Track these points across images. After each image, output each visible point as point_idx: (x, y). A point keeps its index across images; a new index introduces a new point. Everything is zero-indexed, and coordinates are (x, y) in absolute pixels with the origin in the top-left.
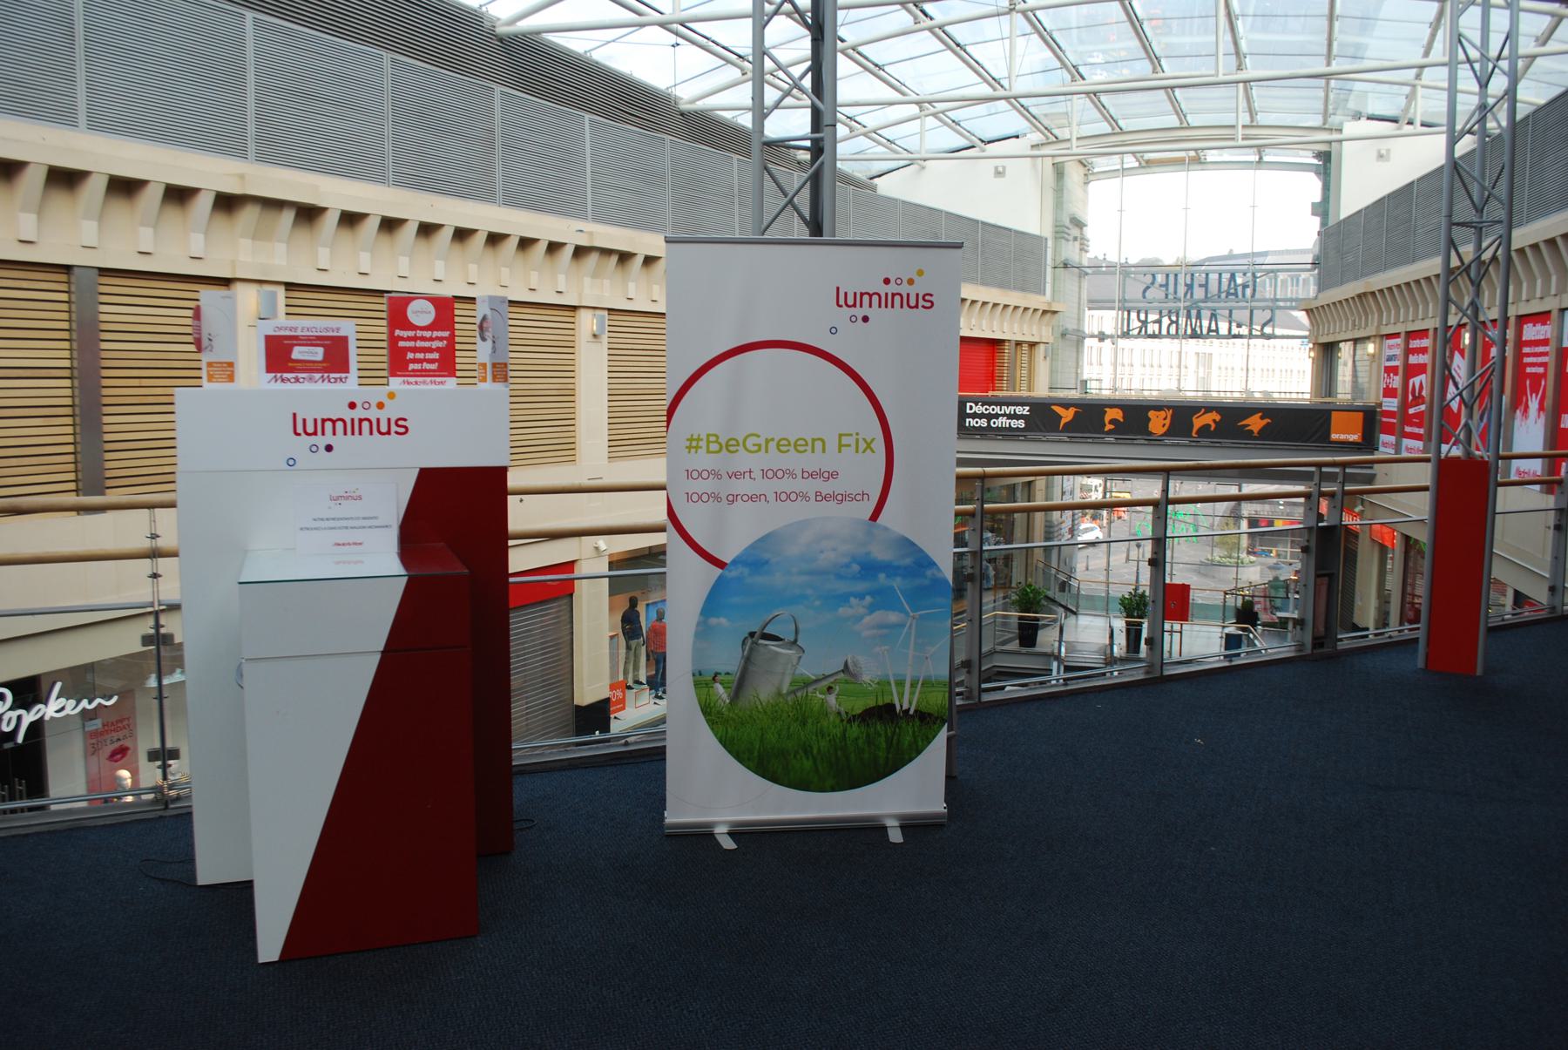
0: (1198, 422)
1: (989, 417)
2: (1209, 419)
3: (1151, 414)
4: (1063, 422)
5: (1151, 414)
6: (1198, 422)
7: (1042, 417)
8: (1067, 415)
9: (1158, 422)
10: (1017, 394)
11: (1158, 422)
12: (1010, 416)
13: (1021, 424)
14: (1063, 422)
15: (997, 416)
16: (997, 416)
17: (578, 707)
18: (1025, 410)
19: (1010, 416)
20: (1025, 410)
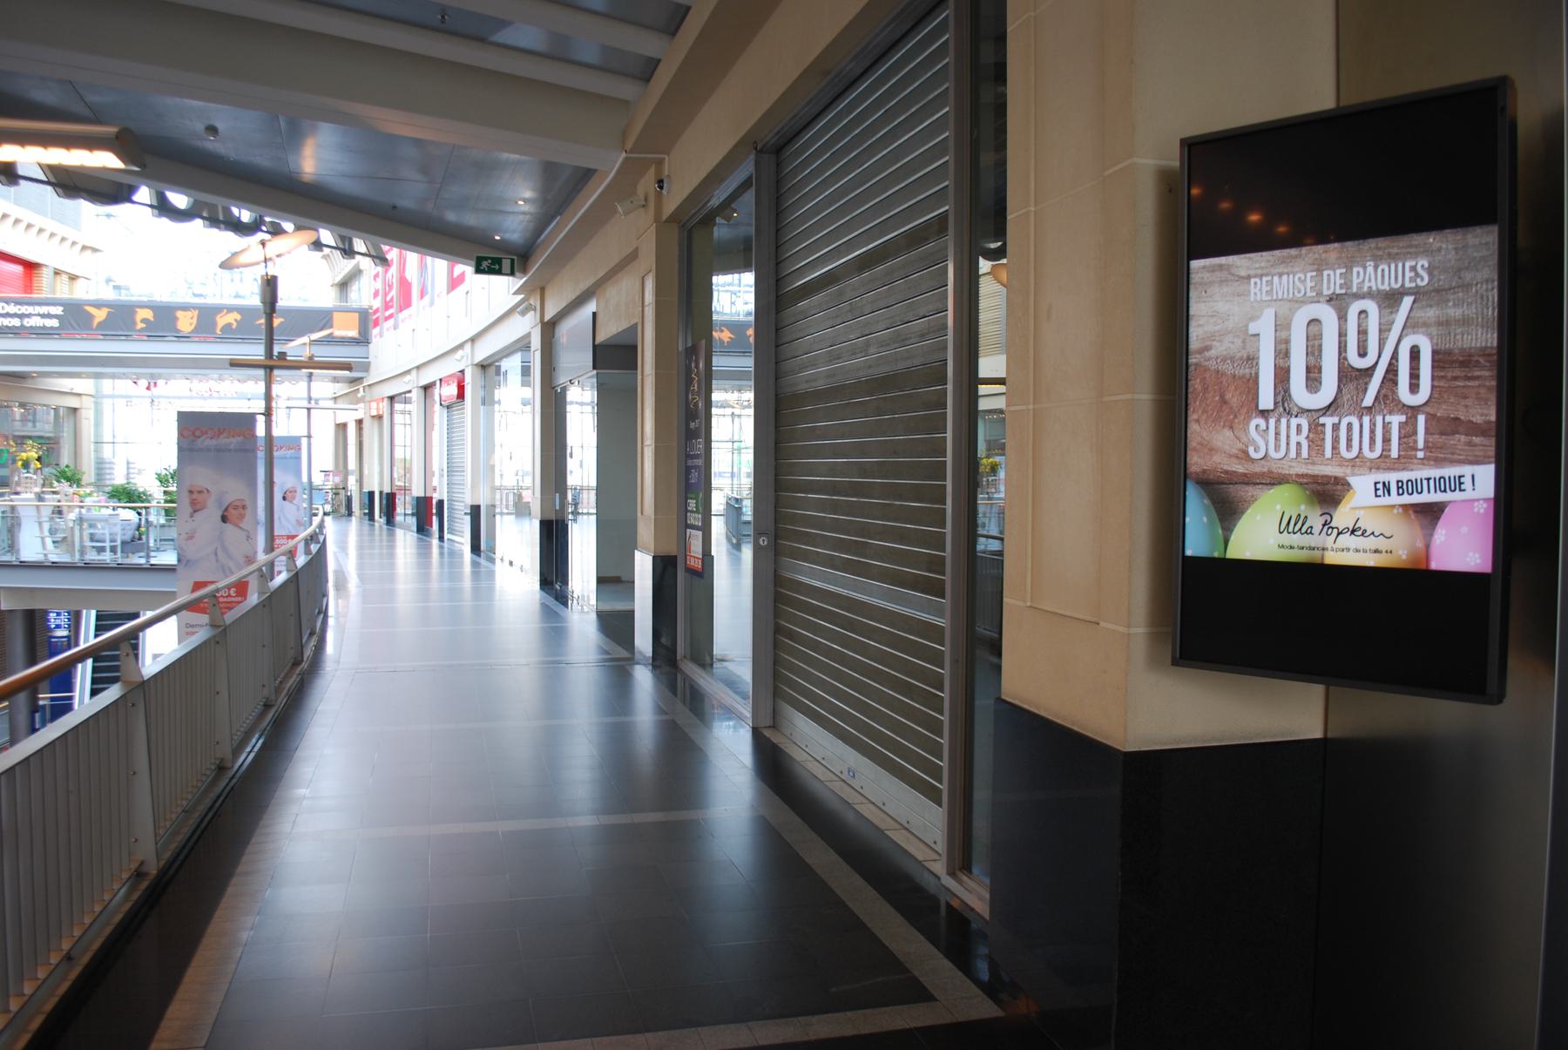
0: (222, 320)
1: (21, 316)
2: (232, 318)
3: (180, 314)
4: (96, 321)
5: (180, 314)
6: (222, 320)
7: (75, 317)
8: (100, 315)
9: (186, 322)
10: (58, 296)
11: (186, 322)
12: (43, 316)
13: (55, 323)
14: (96, 321)
15: (29, 316)
16: (29, 316)
17: (1187, 560)
18: (58, 310)
19: (43, 316)
20: (58, 310)
